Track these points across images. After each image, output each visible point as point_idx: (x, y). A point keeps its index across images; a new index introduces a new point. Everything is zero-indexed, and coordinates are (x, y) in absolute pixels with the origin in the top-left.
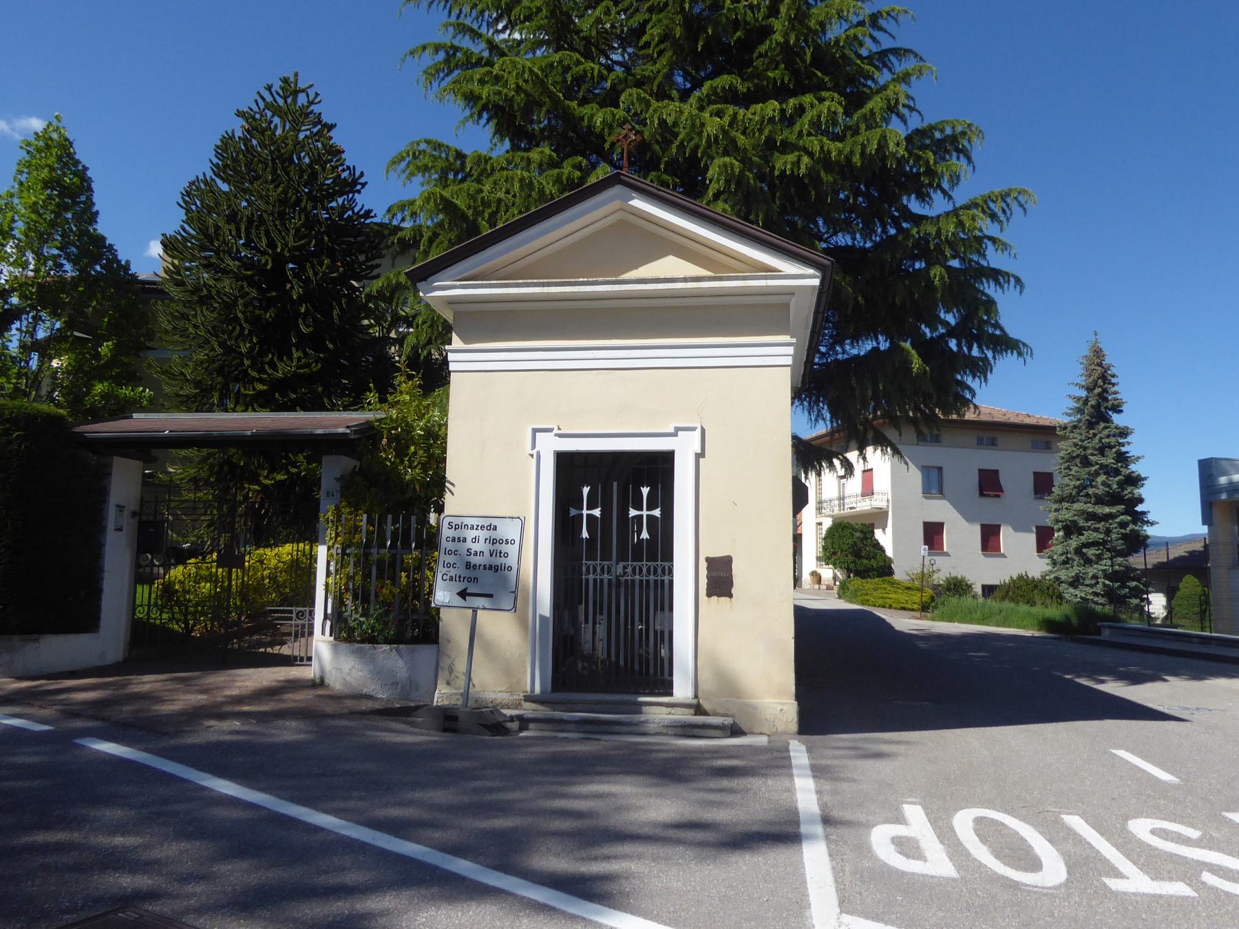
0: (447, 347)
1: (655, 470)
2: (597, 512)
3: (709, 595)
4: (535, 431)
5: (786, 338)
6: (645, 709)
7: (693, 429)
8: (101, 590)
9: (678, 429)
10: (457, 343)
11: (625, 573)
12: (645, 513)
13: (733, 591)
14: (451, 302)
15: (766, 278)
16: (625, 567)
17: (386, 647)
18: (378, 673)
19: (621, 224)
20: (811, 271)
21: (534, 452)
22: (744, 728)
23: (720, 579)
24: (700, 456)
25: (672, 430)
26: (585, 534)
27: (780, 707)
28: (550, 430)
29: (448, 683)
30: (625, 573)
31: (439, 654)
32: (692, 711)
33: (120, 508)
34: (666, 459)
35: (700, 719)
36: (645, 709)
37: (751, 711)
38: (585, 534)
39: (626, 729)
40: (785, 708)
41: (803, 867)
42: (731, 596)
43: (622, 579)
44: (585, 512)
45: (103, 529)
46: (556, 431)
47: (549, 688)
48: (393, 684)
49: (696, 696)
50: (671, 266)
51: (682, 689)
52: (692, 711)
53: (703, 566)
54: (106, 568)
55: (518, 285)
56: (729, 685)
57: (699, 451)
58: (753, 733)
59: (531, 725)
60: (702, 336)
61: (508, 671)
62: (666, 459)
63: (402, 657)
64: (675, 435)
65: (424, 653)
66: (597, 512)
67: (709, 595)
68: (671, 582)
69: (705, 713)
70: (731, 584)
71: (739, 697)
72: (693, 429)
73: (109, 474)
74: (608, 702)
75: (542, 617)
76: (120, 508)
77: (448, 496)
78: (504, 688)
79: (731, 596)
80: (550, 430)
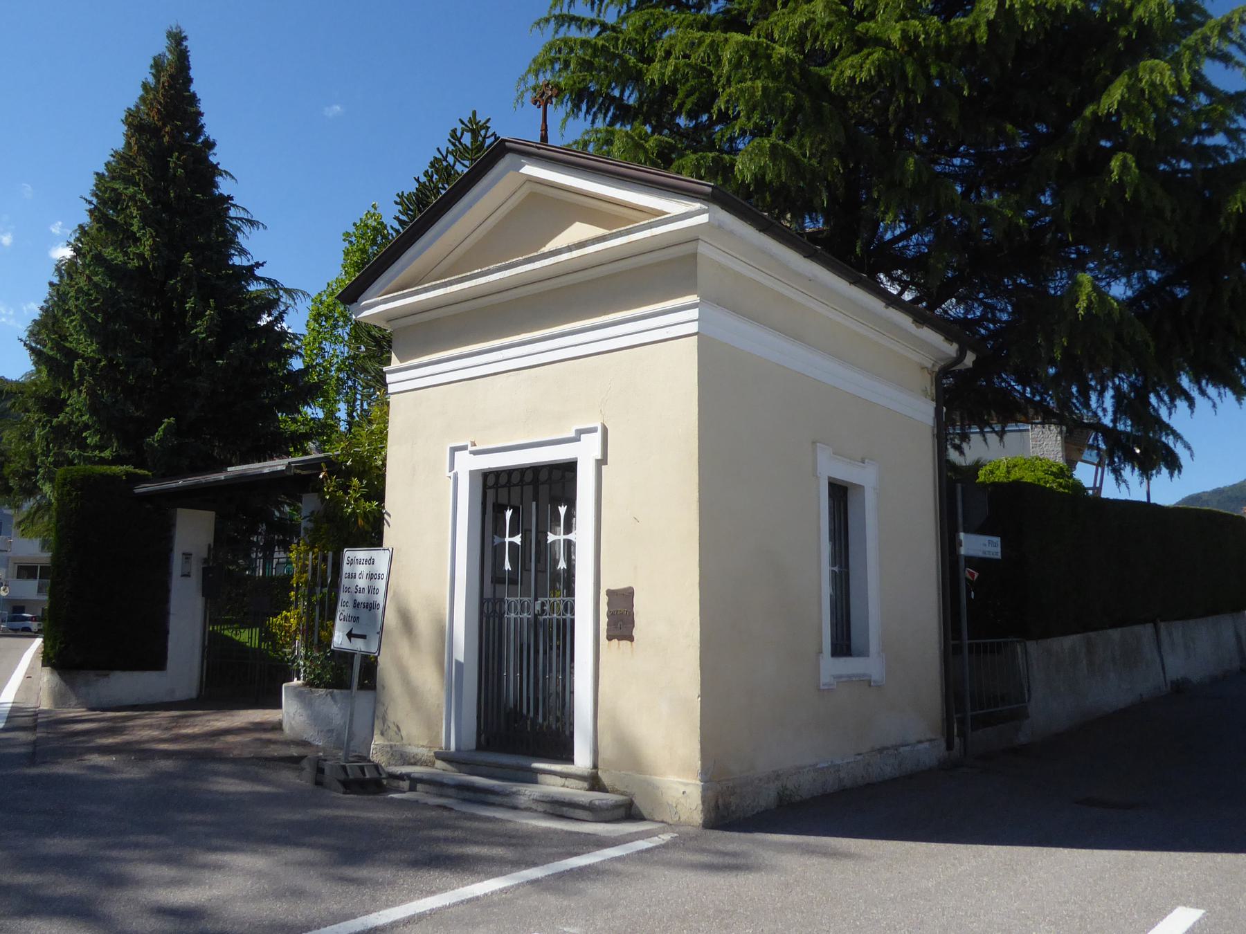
0: (385, 369)
1: (556, 483)
2: (517, 539)
3: (610, 638)
4: (454, 450)
5: (693, 299)
6: (541, 777)
7: (593, 430)
8: (167, 632)
9: (580, 432)
10: (395, 363)
11: (543, 611)
12: (562, 537)
13: (635, 633)
14: (391, 317)
15: (650, 226)
16: (543, 604)
17: (322, 691)
18: (316, 719)
19: (532, 196)
20: (697, 206)
21: (451, 474)
22: (645, 813)
23: (621, 619)
24: (601, 462)
25: (572, 434)
26: (508, 566)
27: (682, 789)
28: (464, 448)
29: (382, 734)
30: (543, 611)
31: (376, 702)
32: (586, 785)
33: (187, 556)
34: (569, 468)
35: (596, 797)
36: (541, 777)
37: (652, 790)
38: (508, 566)
39: (498, 799)
40: (688, 790)
41: (1162, 919)
42: (631, 639)
43: (541, 618)
44: (507, 539)
45: (167, 573)
46: (470, 448)
47: (471, 740)
48: (329, 731)
49: (595, 766)
50: (579, 231)
51: (582, 759)
52: (586, 785)
53: (604, 599)
54: (172, 610)
55: (426, 290)
56: (632, 758)
57: (599, 457)
58: (653, 821)
59: (419, 786)
60: (640, 306)
61: (430, 724)
62: (569, 468)
63: (335, 701)
64: (576, 439)
65: (362, 700)
66: (517, 539)
67: (610, 638)
68: (573, 621)
69: (603, 789)
70: (632, 623)
71: (640, 771)
72: (593, 430)
73: (174, 525)
74: (501, 766)
75: (457, 662)
76: (187, 556)
77: (386, 526)
78: (425, 743)
79: (631, 639)
80: (464, 448)
